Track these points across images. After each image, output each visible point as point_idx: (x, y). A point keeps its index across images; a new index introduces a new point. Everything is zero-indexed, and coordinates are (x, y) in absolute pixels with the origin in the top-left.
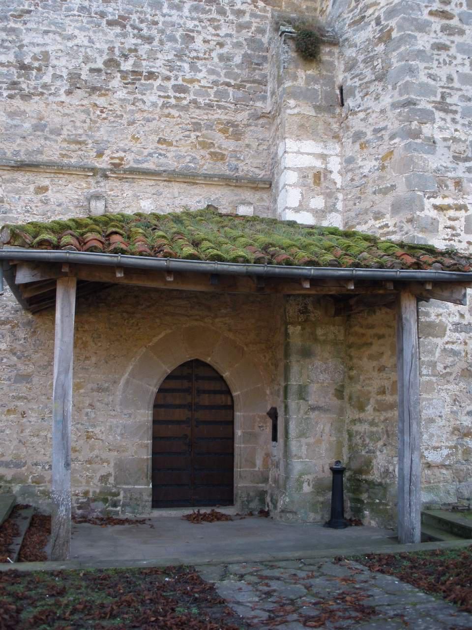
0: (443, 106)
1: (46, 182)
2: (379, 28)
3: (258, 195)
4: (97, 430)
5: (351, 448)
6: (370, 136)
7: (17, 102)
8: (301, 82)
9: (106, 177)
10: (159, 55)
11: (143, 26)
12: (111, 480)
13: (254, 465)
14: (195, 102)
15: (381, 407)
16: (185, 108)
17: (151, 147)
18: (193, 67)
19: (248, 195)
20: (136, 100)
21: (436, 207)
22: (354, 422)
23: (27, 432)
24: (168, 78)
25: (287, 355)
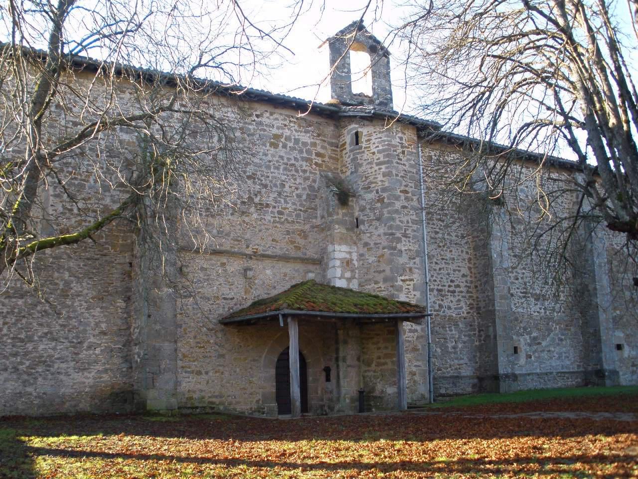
0: (405, 235)
1: (225, 261)
2: (377, 195)
3: (315, 267)
4: (254, 379)
5: (364, 382)
6: (372, 245)
7: (210, 219)
8: (340, 216)
9: (251, 258)
10: (271, 195)
11: (263, 178)
12: (261, 402)
13: (317, 393)
14: (286, 219)
15: (378, 365)
16: (282, 223)
17: (270, 243)
18: (286, 202)
19: (311, 267)
20: (261, 219)
21: (402, 280)
22: (366, 371)
23: (225, 381)
24: (275, 207)
25: (337, 342)
